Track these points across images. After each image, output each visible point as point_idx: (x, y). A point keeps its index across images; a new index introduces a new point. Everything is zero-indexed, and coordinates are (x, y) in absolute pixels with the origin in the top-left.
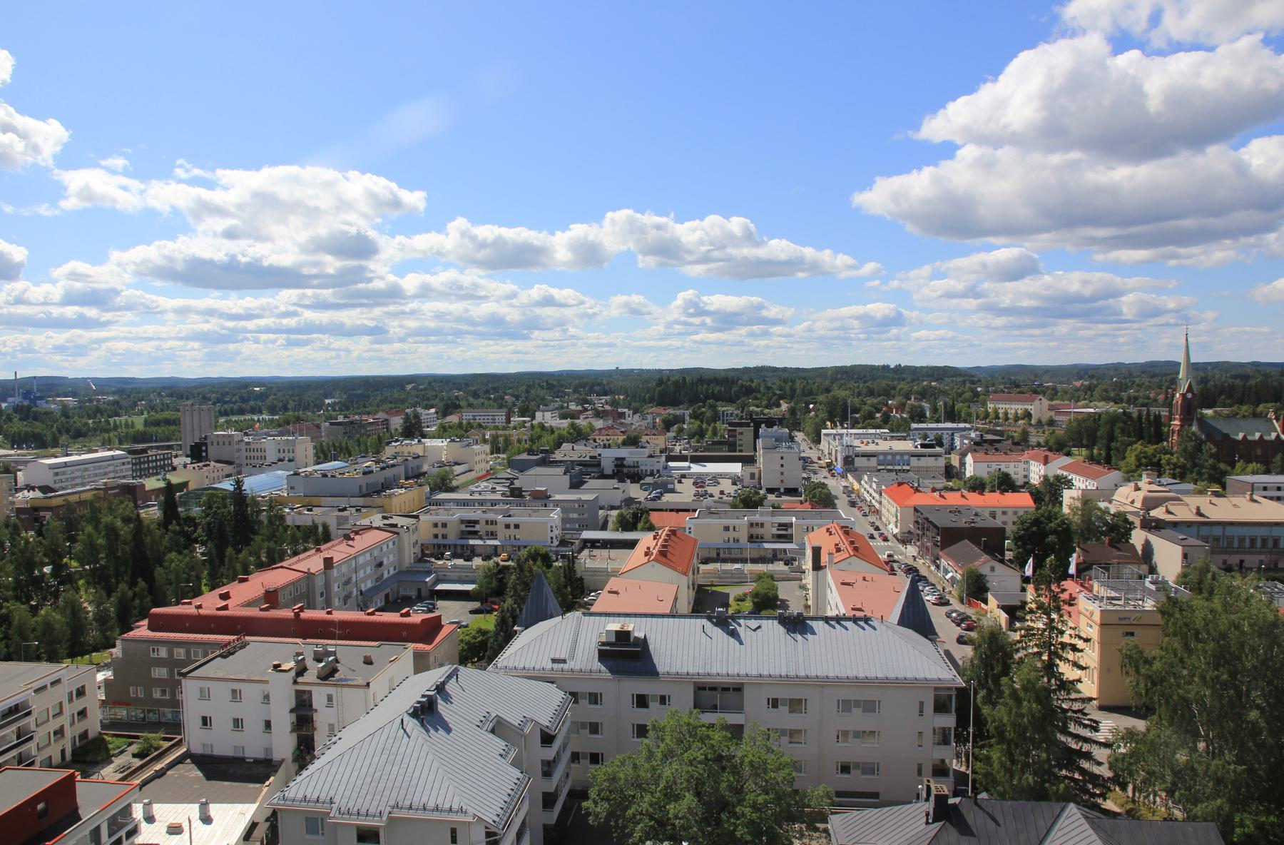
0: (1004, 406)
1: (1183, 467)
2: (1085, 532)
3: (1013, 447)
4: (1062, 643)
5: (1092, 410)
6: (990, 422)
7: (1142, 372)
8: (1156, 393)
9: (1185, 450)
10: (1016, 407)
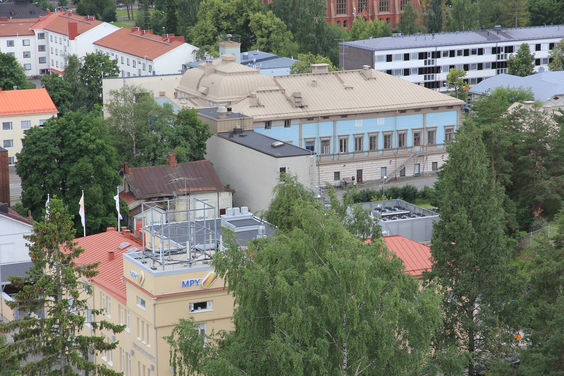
4: (80, 340)
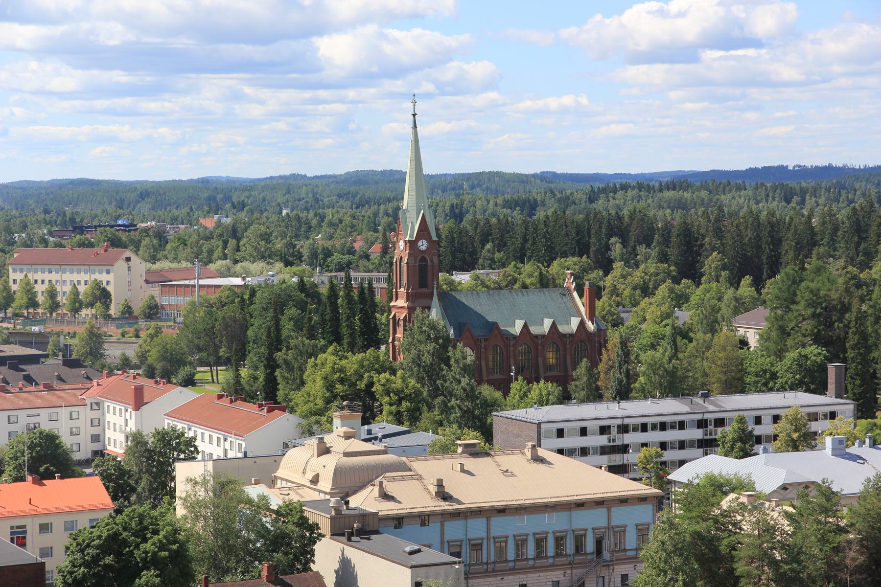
0: (47, 276)
1: (414, 397)
2: (221, 555)
3: (66, 372)
5: (238, 281)
6: (16, 315)
7: (340, 196)
8: (366, 240)
9: (417, 361)
10: (75, 277)
